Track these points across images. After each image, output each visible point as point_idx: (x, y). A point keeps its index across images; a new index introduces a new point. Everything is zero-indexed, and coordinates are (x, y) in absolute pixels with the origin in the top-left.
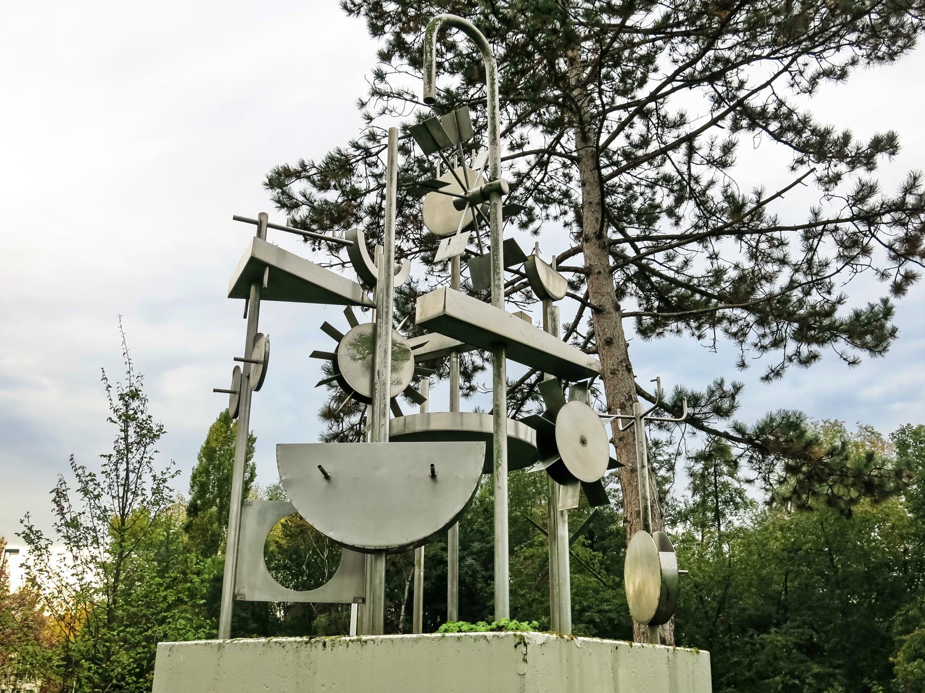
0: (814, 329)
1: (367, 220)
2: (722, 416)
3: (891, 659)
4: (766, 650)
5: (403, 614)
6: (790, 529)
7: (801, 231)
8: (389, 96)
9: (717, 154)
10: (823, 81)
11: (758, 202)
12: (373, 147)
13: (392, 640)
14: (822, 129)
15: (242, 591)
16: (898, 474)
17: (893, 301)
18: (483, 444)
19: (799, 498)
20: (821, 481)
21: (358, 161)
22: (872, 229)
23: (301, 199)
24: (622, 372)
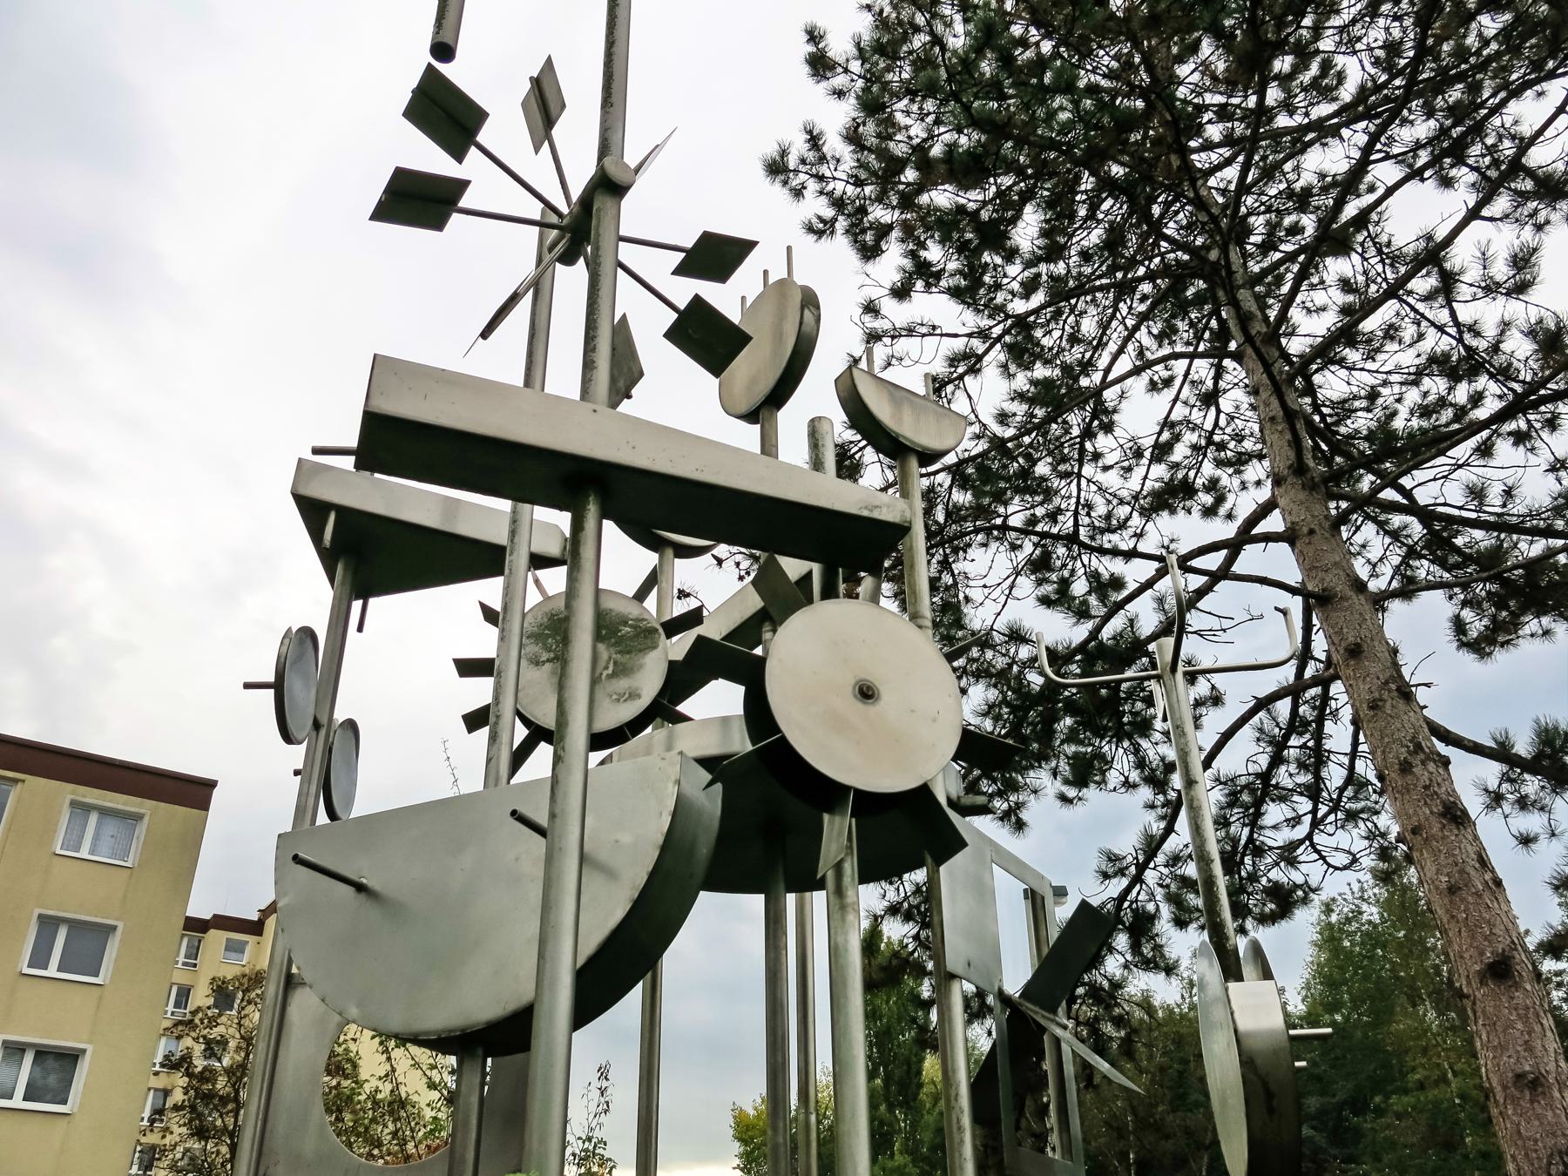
8: (893, 337)
21: (861, 449)
24: (1392, 704)
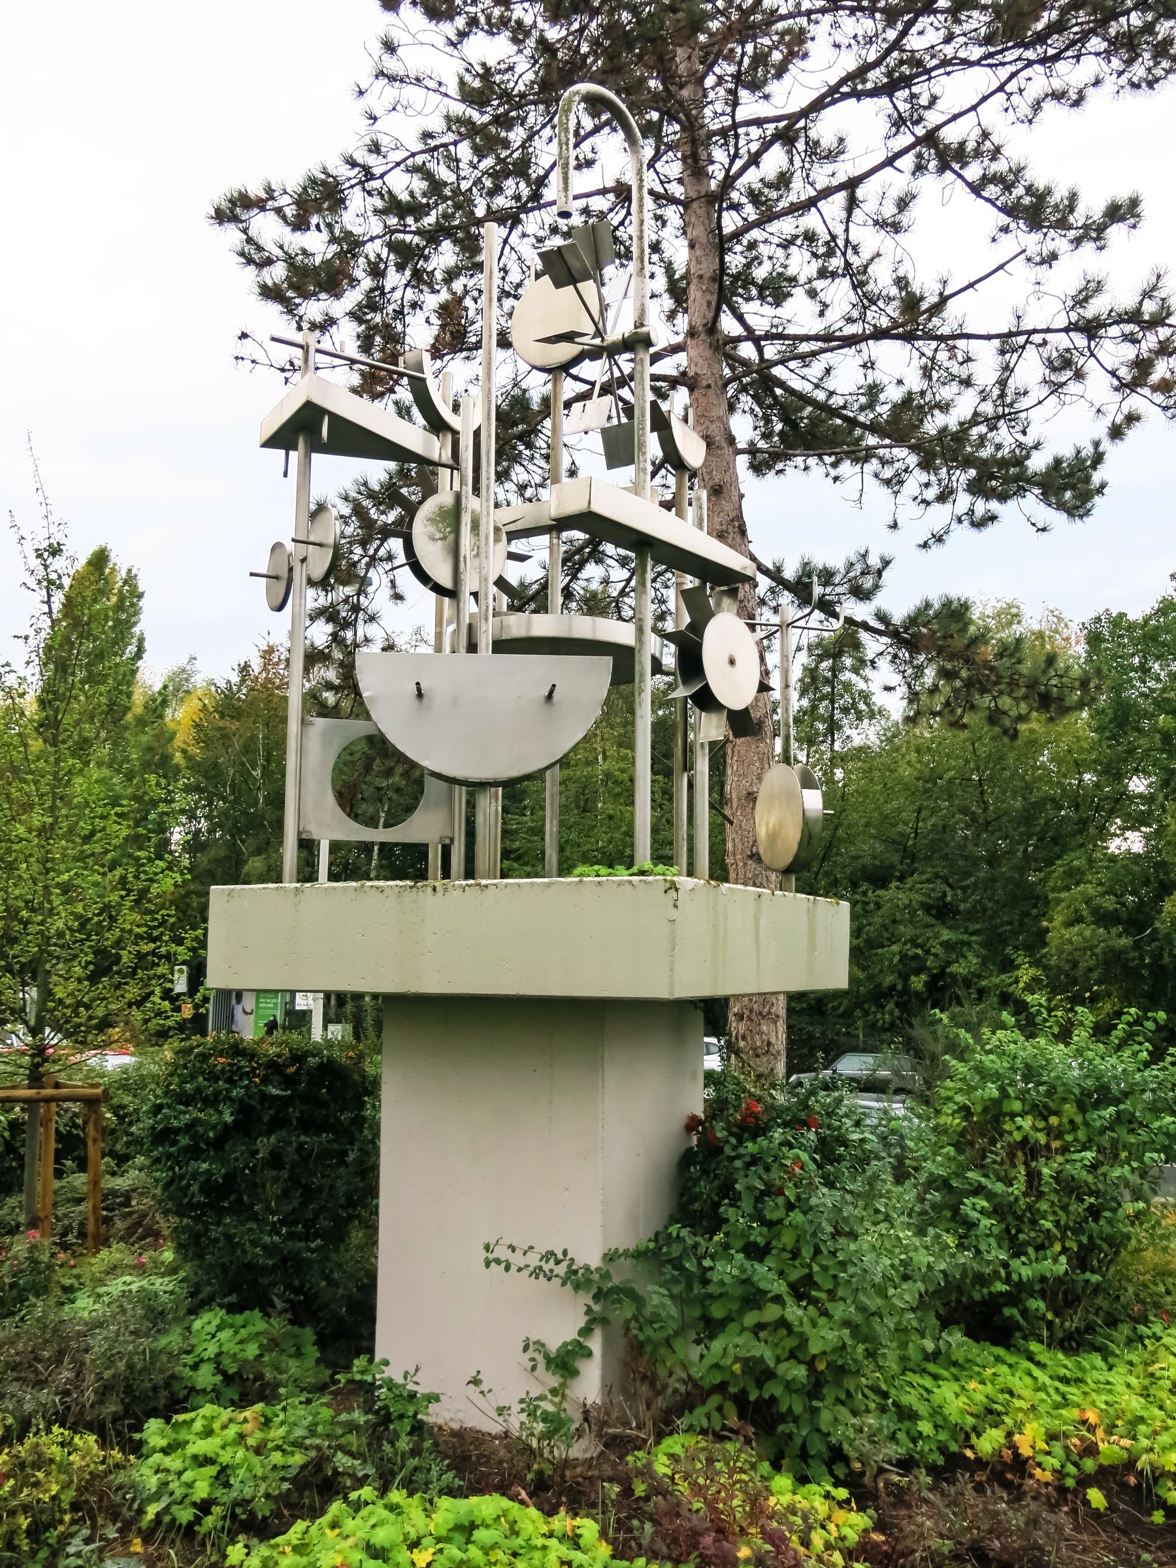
0: (996, 478)
1: (367, 283)
2: (861, 599)
3: (1045, 924)
4: (882, 911)
5: (375, 857)
6: (929, 749)
7: (996, 343)
9: (889, 210)
10: (1049, 106)
11: (941, 294)
12: (377, 164)
13: (519, 885)
14: (1041, 188)
15: (308, 828)
16: (1084, 683)
17: (1106, 445)
18: (607, 661)
19: (952, 712)
20: (983, 691)
21: (352, 187)
22: (1093, 344)
23: (277, 252)
